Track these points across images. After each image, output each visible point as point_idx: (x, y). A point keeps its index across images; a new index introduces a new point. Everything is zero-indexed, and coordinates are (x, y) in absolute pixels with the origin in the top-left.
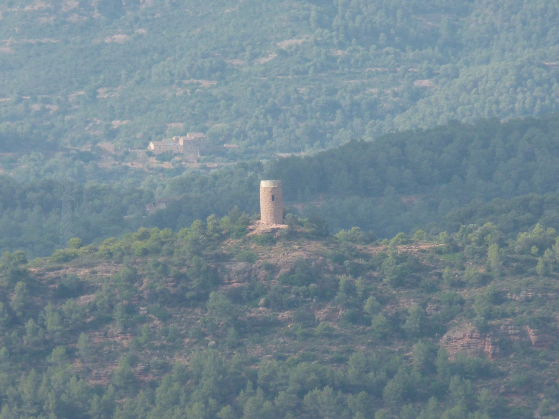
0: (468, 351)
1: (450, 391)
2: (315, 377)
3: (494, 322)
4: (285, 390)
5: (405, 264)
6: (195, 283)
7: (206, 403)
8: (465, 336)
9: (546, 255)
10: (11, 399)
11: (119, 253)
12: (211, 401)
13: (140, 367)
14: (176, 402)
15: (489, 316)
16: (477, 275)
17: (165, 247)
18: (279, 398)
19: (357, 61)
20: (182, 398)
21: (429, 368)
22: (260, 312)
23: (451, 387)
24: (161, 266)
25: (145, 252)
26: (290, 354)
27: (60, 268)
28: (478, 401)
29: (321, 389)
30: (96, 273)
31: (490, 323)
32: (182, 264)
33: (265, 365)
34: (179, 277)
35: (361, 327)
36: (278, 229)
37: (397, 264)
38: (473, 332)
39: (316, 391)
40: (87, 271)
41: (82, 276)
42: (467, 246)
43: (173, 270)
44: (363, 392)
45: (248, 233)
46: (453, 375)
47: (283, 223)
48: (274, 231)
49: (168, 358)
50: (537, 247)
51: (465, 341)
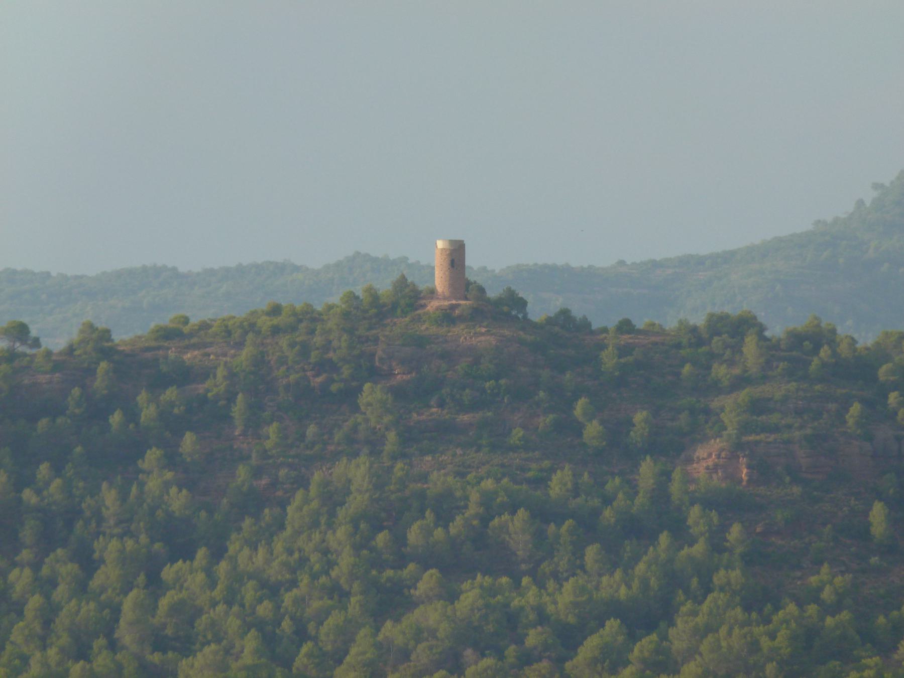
0: (714, 476)
1: (689, 527)
2: (505, 499)
3: (752, 438)
4: (463, 514)
5: (630, 359)
6: (346, 371)
7: (356, 527)
8: (710, 455)
9: (822, 353)
10: (88, 514)
11: (240, 331)
12: (363, 526)
13: (264, 481)
14: (315, 524)
15: (745, 428)
16: (728, 376)
17: (303, 325)
18: (455, 523)
19: (422, 511)
20: (323, 520)
21: (660, 494)
22: (432, 414)
23: (690, 522)
24: (298, 347)
25: (276, 331)
26: (469, 470)
27: (158, 348)
28: (727, 541)
29: (513, 513)
30: (209, 355)
31: (745, 439)
32: (327, 347)
33: (440, 481)
34: (323, 366)
35: (569, 439)
36: (459, 305)
37: (620, 357)
38: (723, 450)
39: (506, 517)
40: (196, 352)
41: (189, 359)
42: (716, 339)
43: (314, 356)
44: (571, 521)
45: (417, 309)
46: (692, 504)
47: (466, 299)
48: (453, 307)
49: (303, 470)
50: (616, 618)
51: (710, 463)
